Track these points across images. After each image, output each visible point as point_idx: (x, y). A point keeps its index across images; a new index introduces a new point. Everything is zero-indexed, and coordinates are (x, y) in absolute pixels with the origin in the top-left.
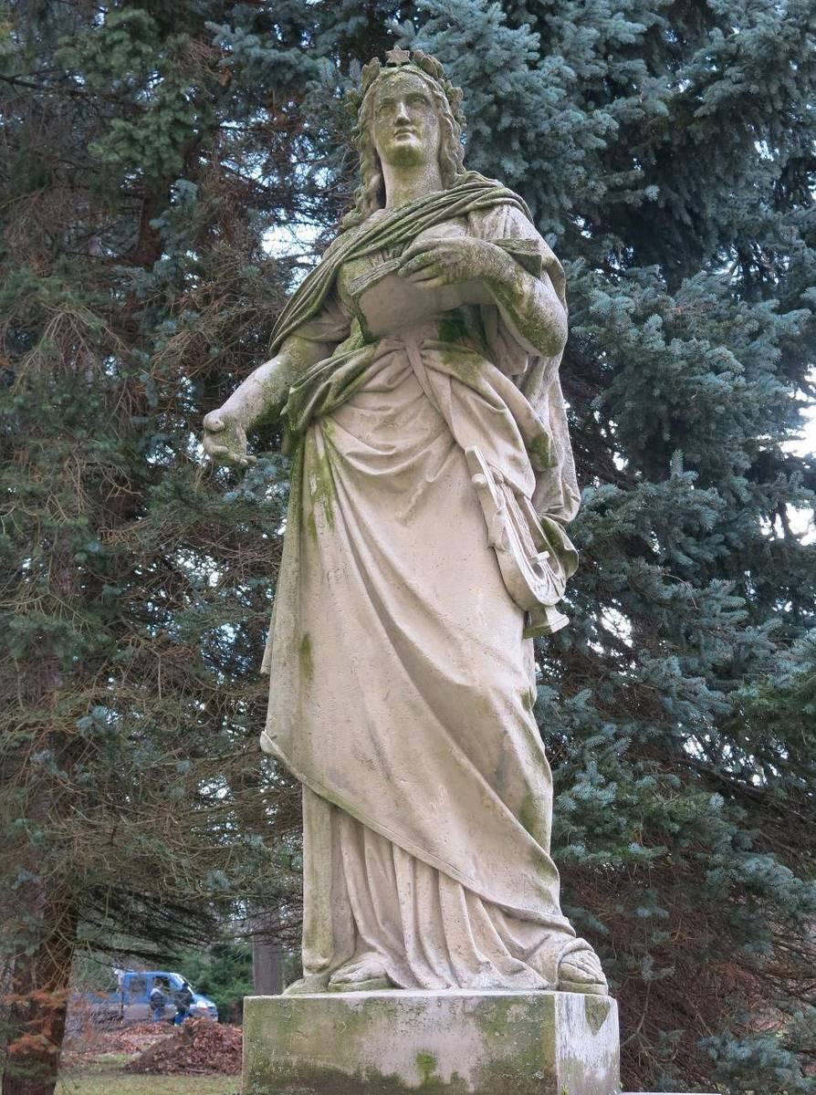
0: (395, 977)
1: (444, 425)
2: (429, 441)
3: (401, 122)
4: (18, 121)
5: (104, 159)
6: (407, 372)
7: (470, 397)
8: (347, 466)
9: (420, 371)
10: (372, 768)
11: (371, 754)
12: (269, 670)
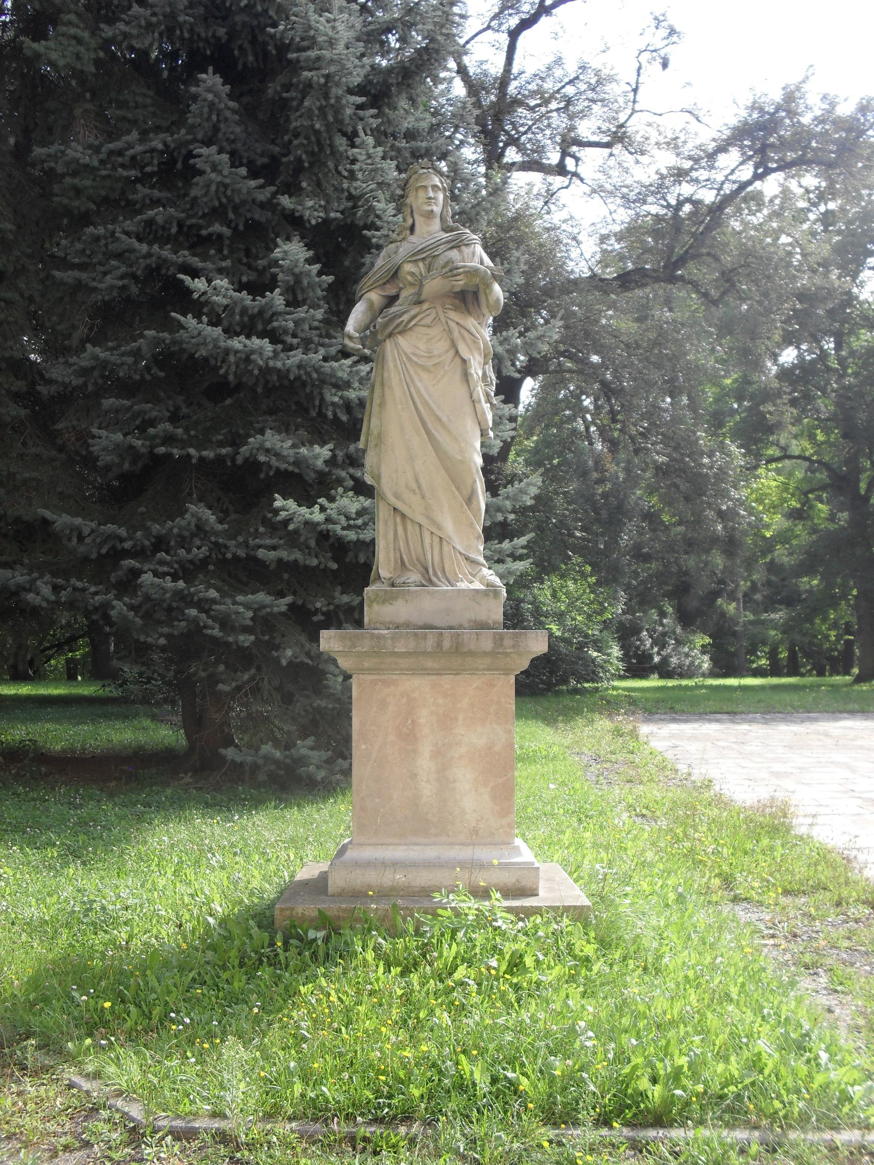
0: (425, 583)
1: (454, 345)
2: (447, 351)
3: (430, 198)
4: (610, 605)
5: (186, 592)
6: (437, 318)
7: (466, 334)
8: (409, 359)
9: (443, 319)
10: (415, 493)
11: (415, 486)
12: (366, 446)
